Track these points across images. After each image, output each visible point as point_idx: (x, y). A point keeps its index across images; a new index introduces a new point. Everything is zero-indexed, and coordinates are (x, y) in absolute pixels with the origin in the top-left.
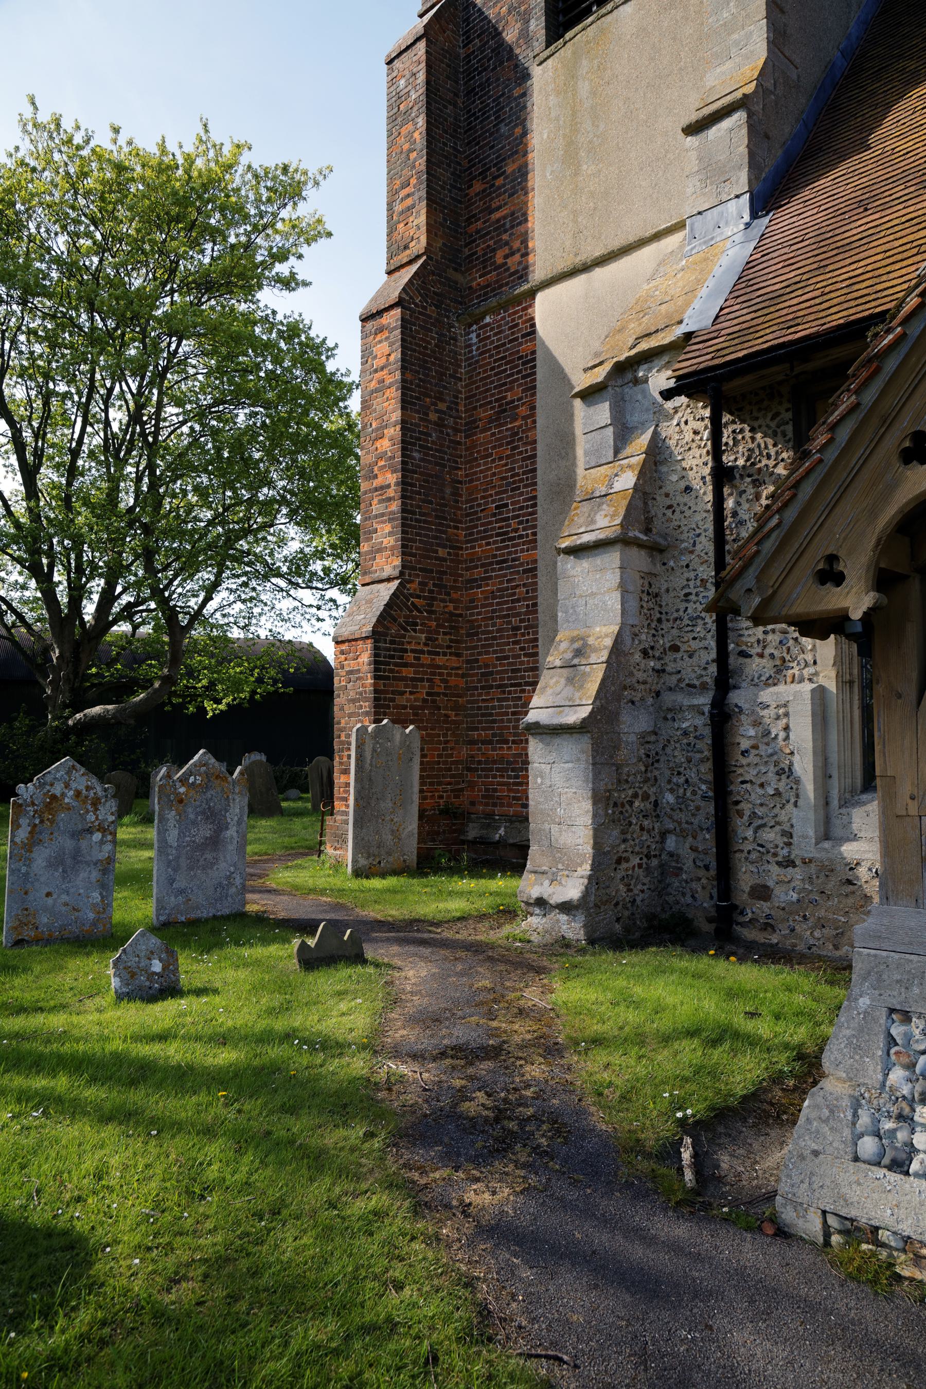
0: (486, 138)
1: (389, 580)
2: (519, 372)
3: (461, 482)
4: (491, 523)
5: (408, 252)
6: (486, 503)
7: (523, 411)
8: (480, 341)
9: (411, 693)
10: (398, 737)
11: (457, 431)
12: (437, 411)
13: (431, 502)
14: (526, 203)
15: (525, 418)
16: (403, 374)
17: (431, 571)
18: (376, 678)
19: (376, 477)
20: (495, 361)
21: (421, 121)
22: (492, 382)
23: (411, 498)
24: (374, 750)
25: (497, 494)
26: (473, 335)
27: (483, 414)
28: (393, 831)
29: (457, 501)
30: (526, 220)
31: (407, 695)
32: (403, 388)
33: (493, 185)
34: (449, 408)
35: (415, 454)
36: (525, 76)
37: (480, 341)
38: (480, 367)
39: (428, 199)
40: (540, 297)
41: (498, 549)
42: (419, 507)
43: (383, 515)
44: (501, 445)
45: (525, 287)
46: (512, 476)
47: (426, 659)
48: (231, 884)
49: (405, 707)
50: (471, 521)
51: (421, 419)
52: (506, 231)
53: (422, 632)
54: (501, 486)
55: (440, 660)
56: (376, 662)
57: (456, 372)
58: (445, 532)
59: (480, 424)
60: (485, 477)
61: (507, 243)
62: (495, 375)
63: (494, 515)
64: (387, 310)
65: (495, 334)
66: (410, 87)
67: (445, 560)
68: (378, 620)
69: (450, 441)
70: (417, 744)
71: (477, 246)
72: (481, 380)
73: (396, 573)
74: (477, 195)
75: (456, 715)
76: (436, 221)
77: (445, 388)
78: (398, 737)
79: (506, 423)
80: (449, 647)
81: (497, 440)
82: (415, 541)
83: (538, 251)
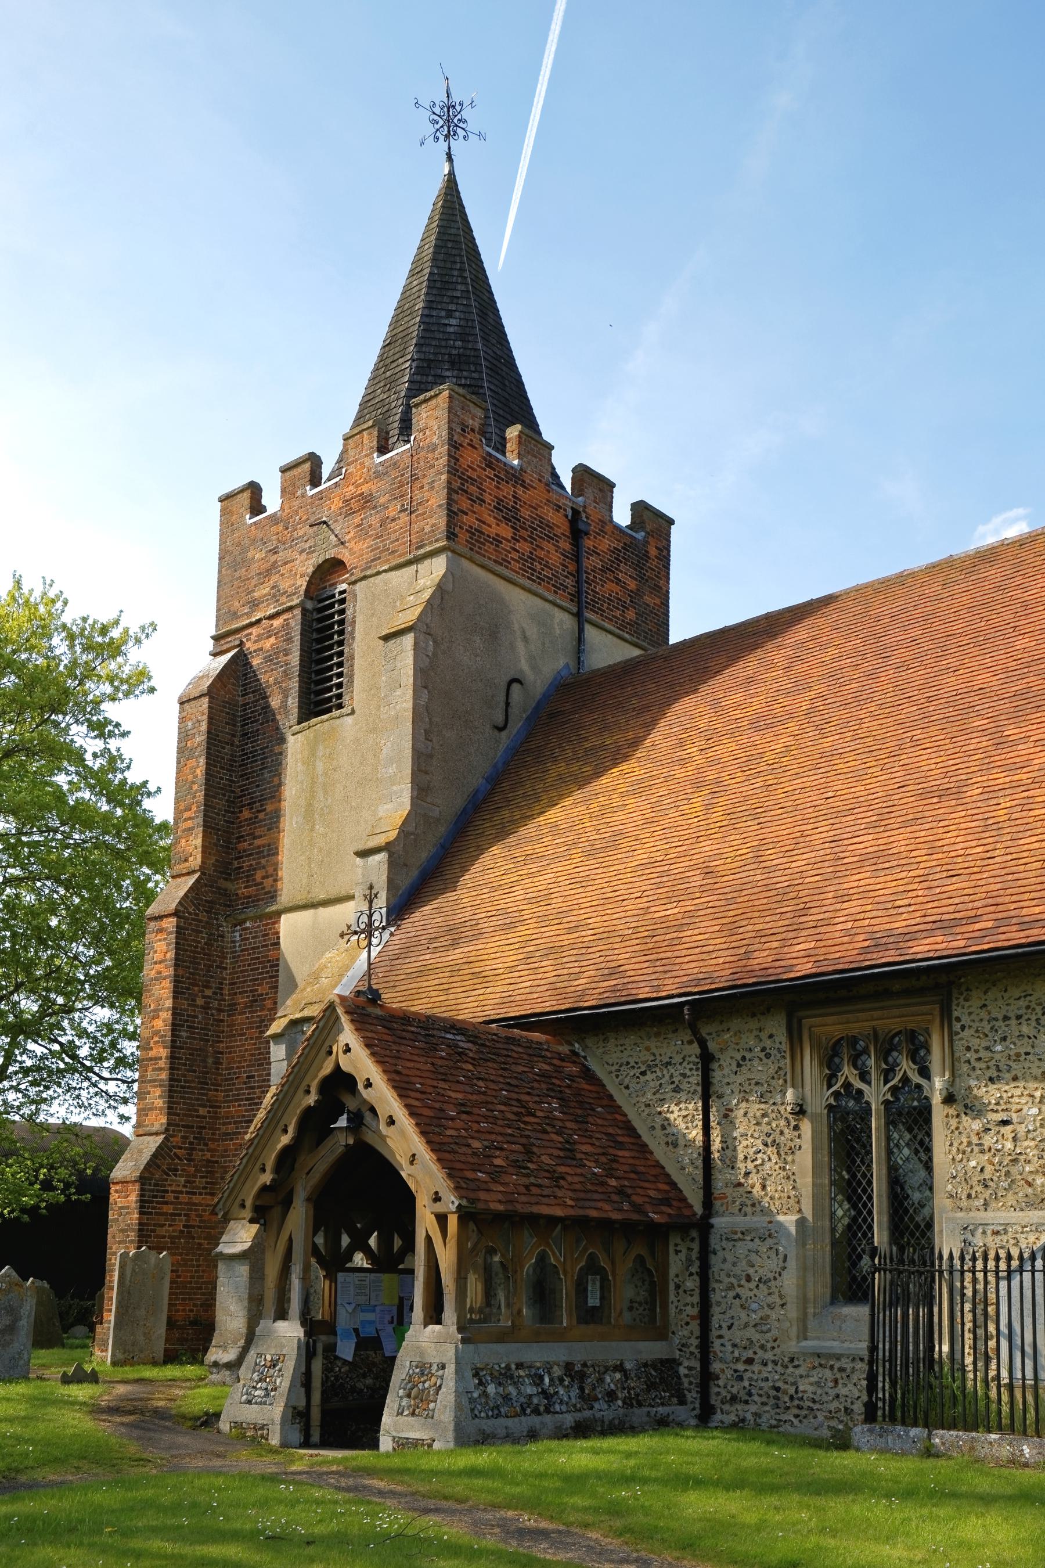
0: (253, 777)
1: (157, 1134)
2: (267, 972)
3: (222, 1053)
4: (242, 1089)
5: (187, 864)
6: (240, 1073)
7: (268, 1003)
8: (242, 940)
9: (170, 1225)
10: (153, 1261)
11: (220, 1011)
12: (204, 997)
13: (195, 1071)
14: (278, 839)
15: (270, 1010)
16: (175, 970)
17: (193, 1127)
18: (140, 1213)
19: (151, 1049)
20: (252, 959)
21: (202, 761)
22: (248, 976)
23: (178, 1069)
24: (133, 1270)
25: (248, 1066)
26: (237, 934)
27: (242, 1000)
28: (145, 1334)
29: (218, 1069)
30: (277, 854)
31: (167, 1227)
32: (175, 981)
33: (257, 817)
34: (215, 993)
35: (184, 1034)
36: (282, 740)
37: (242, 940)
38: (242, 961)
39: (204, 826)
40: (283, 917)
41: (246, 1111)
42: (185, 1076)
43: (155, 1081)
44: (252, 1028)
45: (273, 908)
46: (259, 1054)
47: (184, 1198)
48: (20, 1358)
49: (164, 1237)
50: (229, 1085)
51: (189, 1005)
52: (264, 857)
53: (181, 1176)
54: (250, 1061)
55: (196, 1199)
56: (141, 1201)
57: (222, 962)
58: (206, 1095)
59: (238, 1007)
60: (240, 1051)
61: (264, 867)
62: (252, 970)
63: (245, 1083)
64: (166, 916)
65: (253, 938)
66: (195, 731)
67: (204, 1117)
68: (145, 1168)
69: (214, 1020)
70: (168, 1267)
71: (244, 862)
72: (241, 972)
73: (163, 1129)
74: (246, 820)
75: (208, 1244)
76: (210, 843)
77: (212, 977)
78: (153, 1261)
79: (256, 1011)
80: (205, 1188)
81: (250, 1023)
82: (179, 1103)
83: (285, 881)
